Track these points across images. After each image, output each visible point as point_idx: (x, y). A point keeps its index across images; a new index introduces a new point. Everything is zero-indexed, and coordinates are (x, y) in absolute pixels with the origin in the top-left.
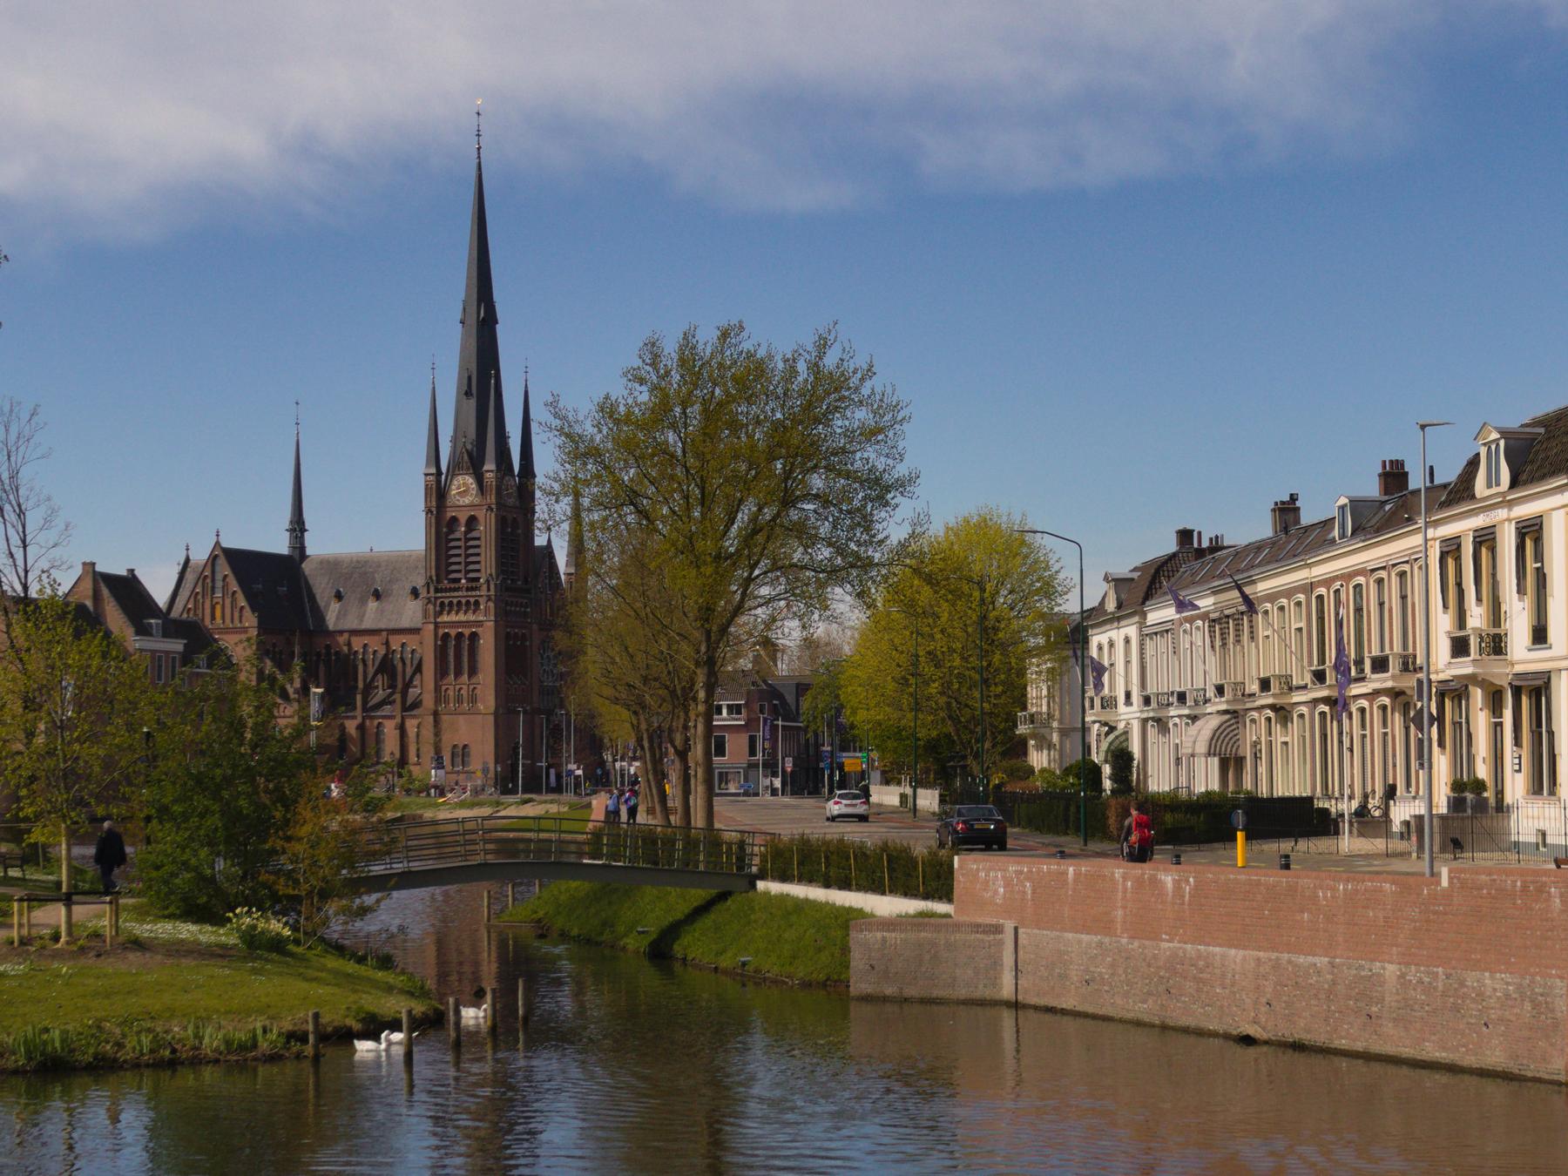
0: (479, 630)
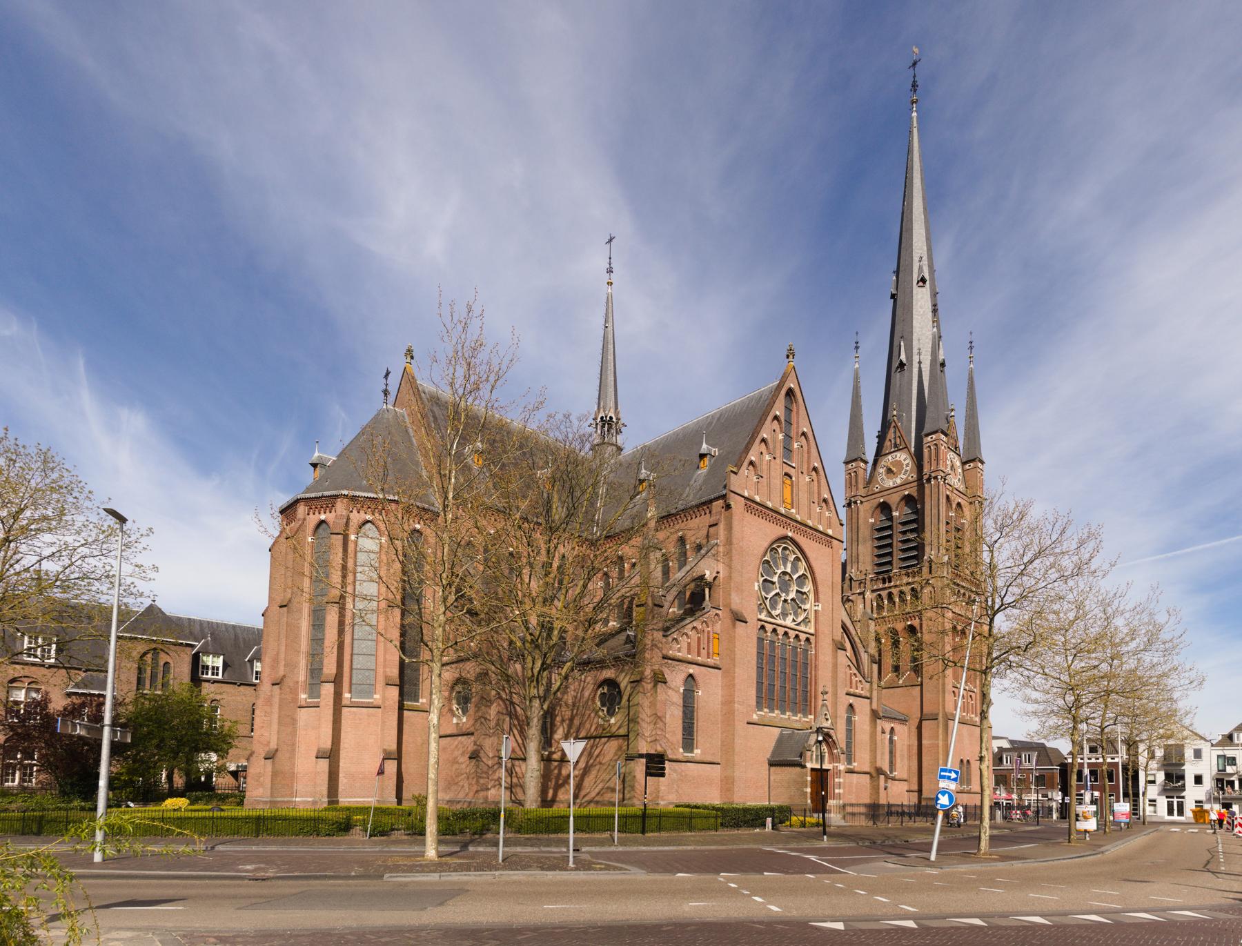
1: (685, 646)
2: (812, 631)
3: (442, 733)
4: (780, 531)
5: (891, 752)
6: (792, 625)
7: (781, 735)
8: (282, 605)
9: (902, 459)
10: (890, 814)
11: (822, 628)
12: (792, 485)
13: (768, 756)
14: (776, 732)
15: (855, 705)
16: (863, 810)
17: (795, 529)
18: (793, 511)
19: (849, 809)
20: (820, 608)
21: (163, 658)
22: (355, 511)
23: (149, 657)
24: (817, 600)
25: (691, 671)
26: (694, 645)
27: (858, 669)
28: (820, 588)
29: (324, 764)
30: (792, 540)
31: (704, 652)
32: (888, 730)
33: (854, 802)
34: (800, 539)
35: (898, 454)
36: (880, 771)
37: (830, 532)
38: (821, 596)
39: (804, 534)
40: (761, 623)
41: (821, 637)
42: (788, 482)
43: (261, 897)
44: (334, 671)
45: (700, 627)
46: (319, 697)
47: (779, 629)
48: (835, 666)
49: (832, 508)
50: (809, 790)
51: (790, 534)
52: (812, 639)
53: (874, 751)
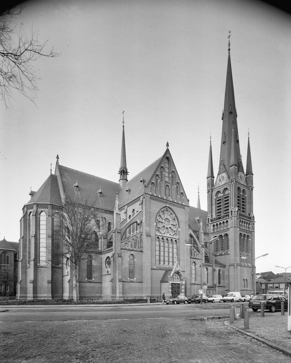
1: (130, 245)
2: (177, 238)
3: (101, 284)
4: (164, 205)
6: (170, 236)
8: (24, 238)
11: (181, 236)
12: (169, 189)
15: (196, 262)
17: (169, 204)
20: (180, 230)
21: (7, 255)
22: (39, 208)
23: (3, 255)
24: (179, 227)
25: (132, 253)
26: (133, 244)
28: (180, 223)
29: (49, 53)
30: (169, 207)
34: (172, 207)
35: (223, 174)
37: (184, 204)
38: (181, 226)
39: (174, 205)
40: (157, 236)
41: (181, 240)
42: (168, 188)
44: (34, 234)
45: (135, 239)
46: (281, 309)
47: (164, 238)
51: (168, 206)
52: (177, 241)
53: (213, 279)
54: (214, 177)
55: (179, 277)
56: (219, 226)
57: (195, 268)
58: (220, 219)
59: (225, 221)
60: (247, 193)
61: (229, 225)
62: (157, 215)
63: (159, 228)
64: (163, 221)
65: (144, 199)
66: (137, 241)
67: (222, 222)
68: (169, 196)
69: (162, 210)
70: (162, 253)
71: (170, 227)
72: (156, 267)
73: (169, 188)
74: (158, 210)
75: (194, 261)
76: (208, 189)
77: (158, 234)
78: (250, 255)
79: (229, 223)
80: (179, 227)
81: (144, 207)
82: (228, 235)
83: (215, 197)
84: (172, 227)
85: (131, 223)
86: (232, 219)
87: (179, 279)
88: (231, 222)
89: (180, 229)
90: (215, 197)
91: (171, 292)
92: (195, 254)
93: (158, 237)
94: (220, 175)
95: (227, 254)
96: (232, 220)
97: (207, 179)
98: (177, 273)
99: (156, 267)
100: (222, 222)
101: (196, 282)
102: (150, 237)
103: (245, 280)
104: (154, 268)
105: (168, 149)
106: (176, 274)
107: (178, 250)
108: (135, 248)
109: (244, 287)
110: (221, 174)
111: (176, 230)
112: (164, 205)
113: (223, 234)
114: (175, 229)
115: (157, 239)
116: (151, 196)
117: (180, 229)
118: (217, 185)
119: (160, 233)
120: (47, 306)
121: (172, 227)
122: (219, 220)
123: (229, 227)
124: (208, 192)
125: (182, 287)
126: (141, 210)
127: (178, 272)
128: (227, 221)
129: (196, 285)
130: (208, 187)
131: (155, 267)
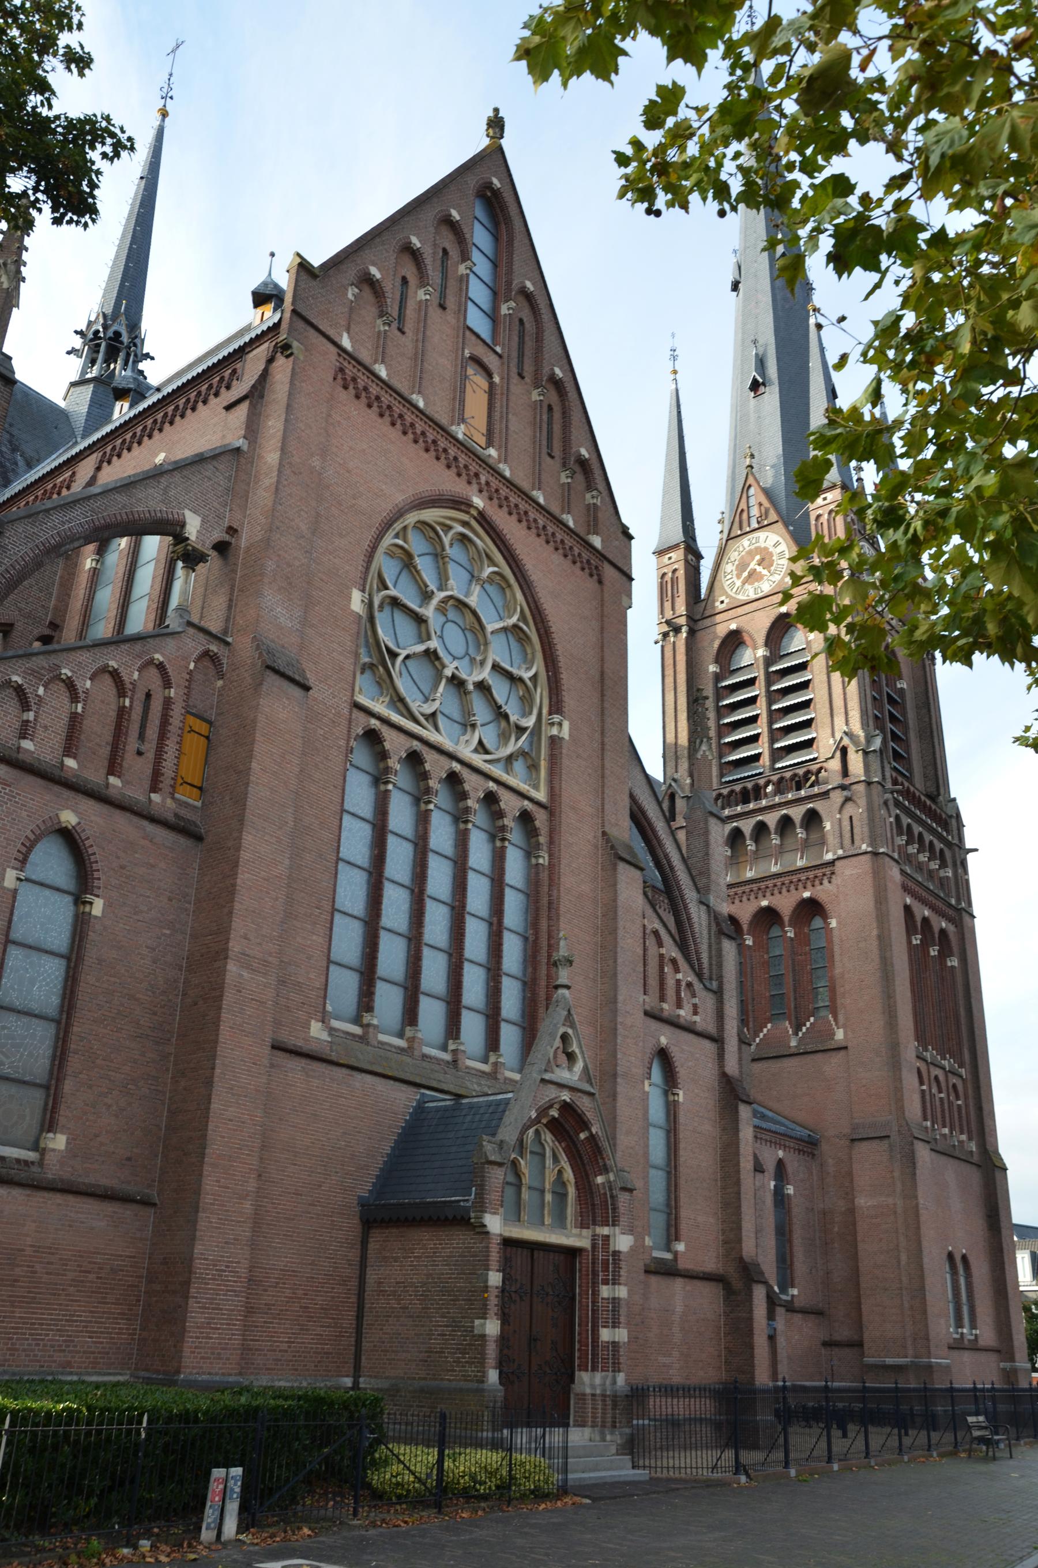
0: (823, 892)
2: (541, 796)
4: (449, 483)
5: (845, 699)
6: (478, 760)
7: (420, 1109)
9: (770, 544)
10: (786, 1416)
13: (364, 1188)
14: (404, 1099)
15: (676, 1053)
16: (704, 1407)
18: (493, 452)
19: (659, 1406)
24: (556, 706)
25: (68, 818)
27: (683, 945)
31: (139, 768)
32: (770, 1166)
33: (676, 1377)
35: (762, 535)
36: (750, 1273)
37: (597, 541)
38: (569, 700)
40: (362, 723)
41: (568, 819)
43: (593, 1263)
47: (431, 759)
48: (611, 911)
49: (601, 486)
50: (492, 1327)
52: (541, 819)
54: (699, 557)
55: (569, 1175)
56: (751, 846)
57: (672, 1109)
58: (757, 798)
59: (797, 813)
60: (905, 669)
61: (832, 840)
62: (374, 548)
63: (394, 655)
64: (429, 612)
65: (281, 360)
66: (157, 706)
67: (771, 819)
68: (490, 443)
69: (430, 515)
70: (395, 906)
71: (482, 687)
72: (332, 1031)
73: (492, 385)
74: (400, 498)
75: (663, 1040)
76: (662, 612)
77: (380, 707)
78: (963, 1071)
79: (828, 826)
80: (556, 706)
81: (274, 425)
82: (828, 907)
83: (713, 668)
84: (500, 691)
85: (116, 508)
86: (848, 799)
87: (571, 1191)
88: (846, 823)
89: (566, 725)
90: (713, 668)
91: (492, 1351)
92: (670, 983)
93: (372, 737)
94: (745, 542)
95: (822, 1047)
96: (850, 809)
97: (654, 558)
98: (554, 1126)
99: (332, 1031)
100: (771, 819)
101: (681, 1247)
102: (297, 692)
103: (958, 1259)
104: (306, 1047)
105: (501, 149)
106: (548, 1137)
107: (544, 913)
108: (113, 767)
109: (959, 1324)
110: (750, 536)
111: (530, 722)
112: (449, 483)
113: (785, 903)
114: (526, 714)
115: (362, 756)
116: (350, 370)
117: (566, 725)
118: (728, 596)
119: (399, 702)
120: (744, 1208)
121: (500, 691)
122: (752, 806)
123: (829, 856)
124: (665, 635)
125: (605, 1291)
126: (240, 442)
127: (566, 1108)
128: (813, 818)
129: (679, 1283)
130: (668, 605)
131: (316, 1030)
